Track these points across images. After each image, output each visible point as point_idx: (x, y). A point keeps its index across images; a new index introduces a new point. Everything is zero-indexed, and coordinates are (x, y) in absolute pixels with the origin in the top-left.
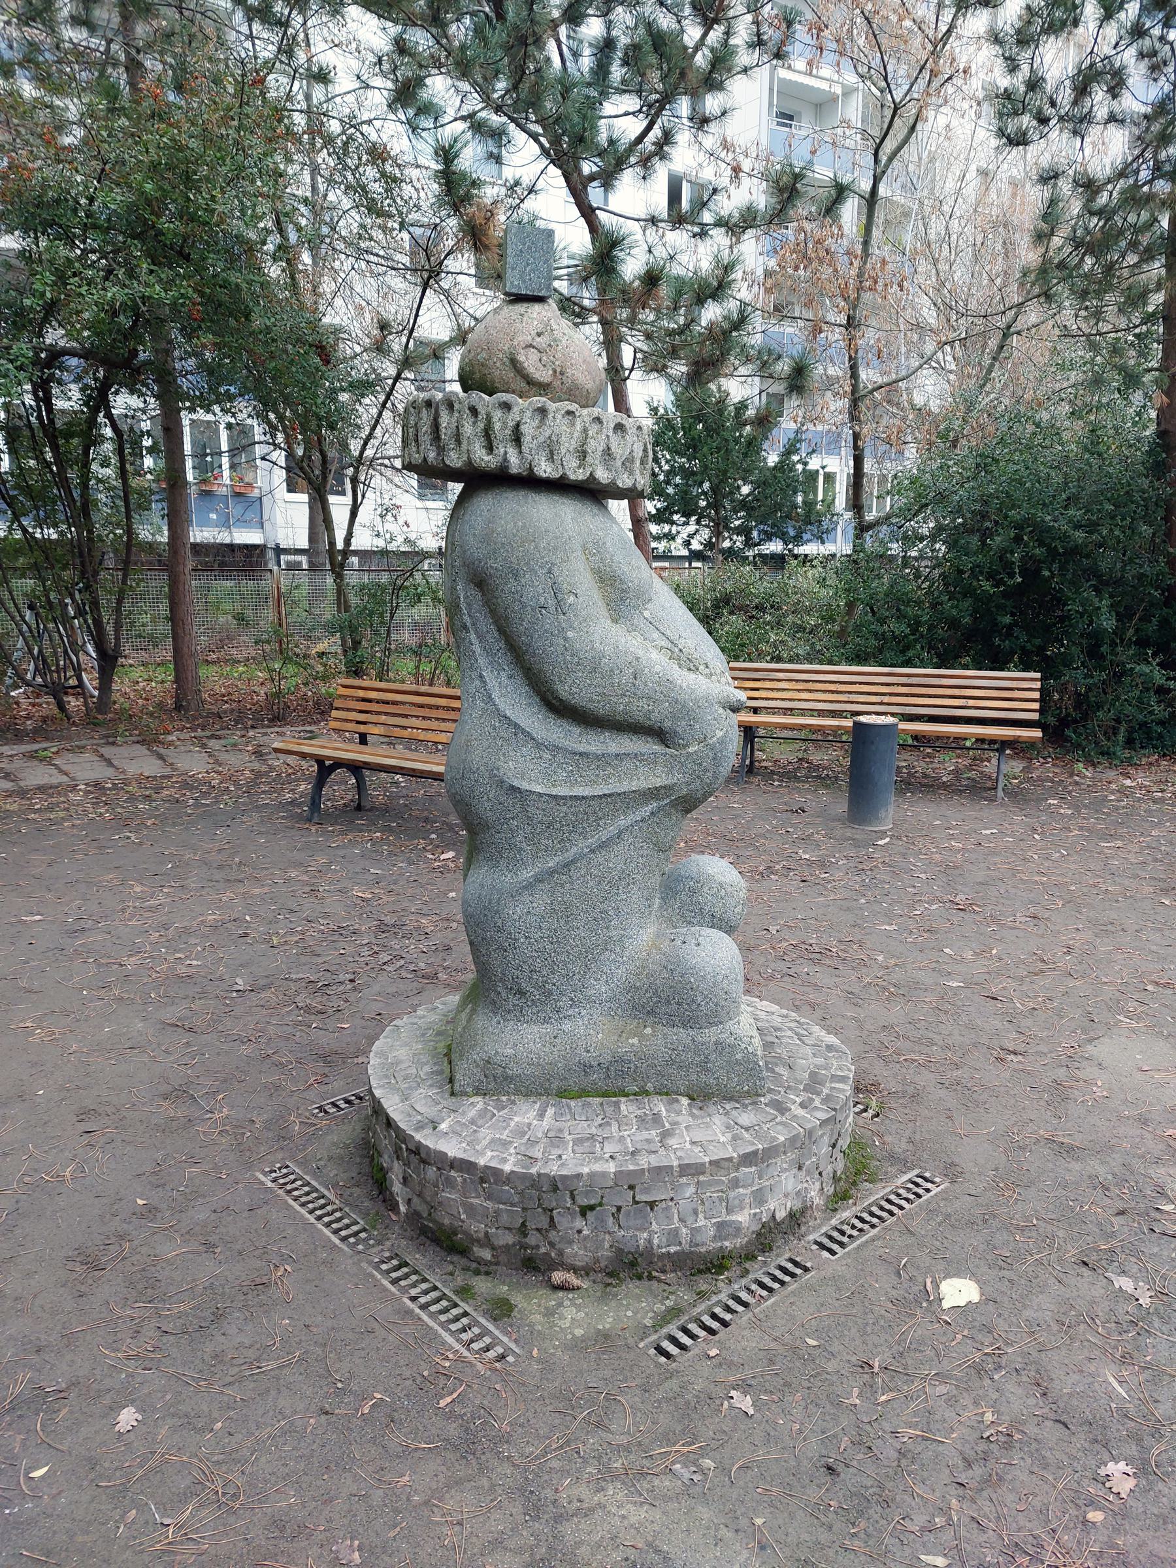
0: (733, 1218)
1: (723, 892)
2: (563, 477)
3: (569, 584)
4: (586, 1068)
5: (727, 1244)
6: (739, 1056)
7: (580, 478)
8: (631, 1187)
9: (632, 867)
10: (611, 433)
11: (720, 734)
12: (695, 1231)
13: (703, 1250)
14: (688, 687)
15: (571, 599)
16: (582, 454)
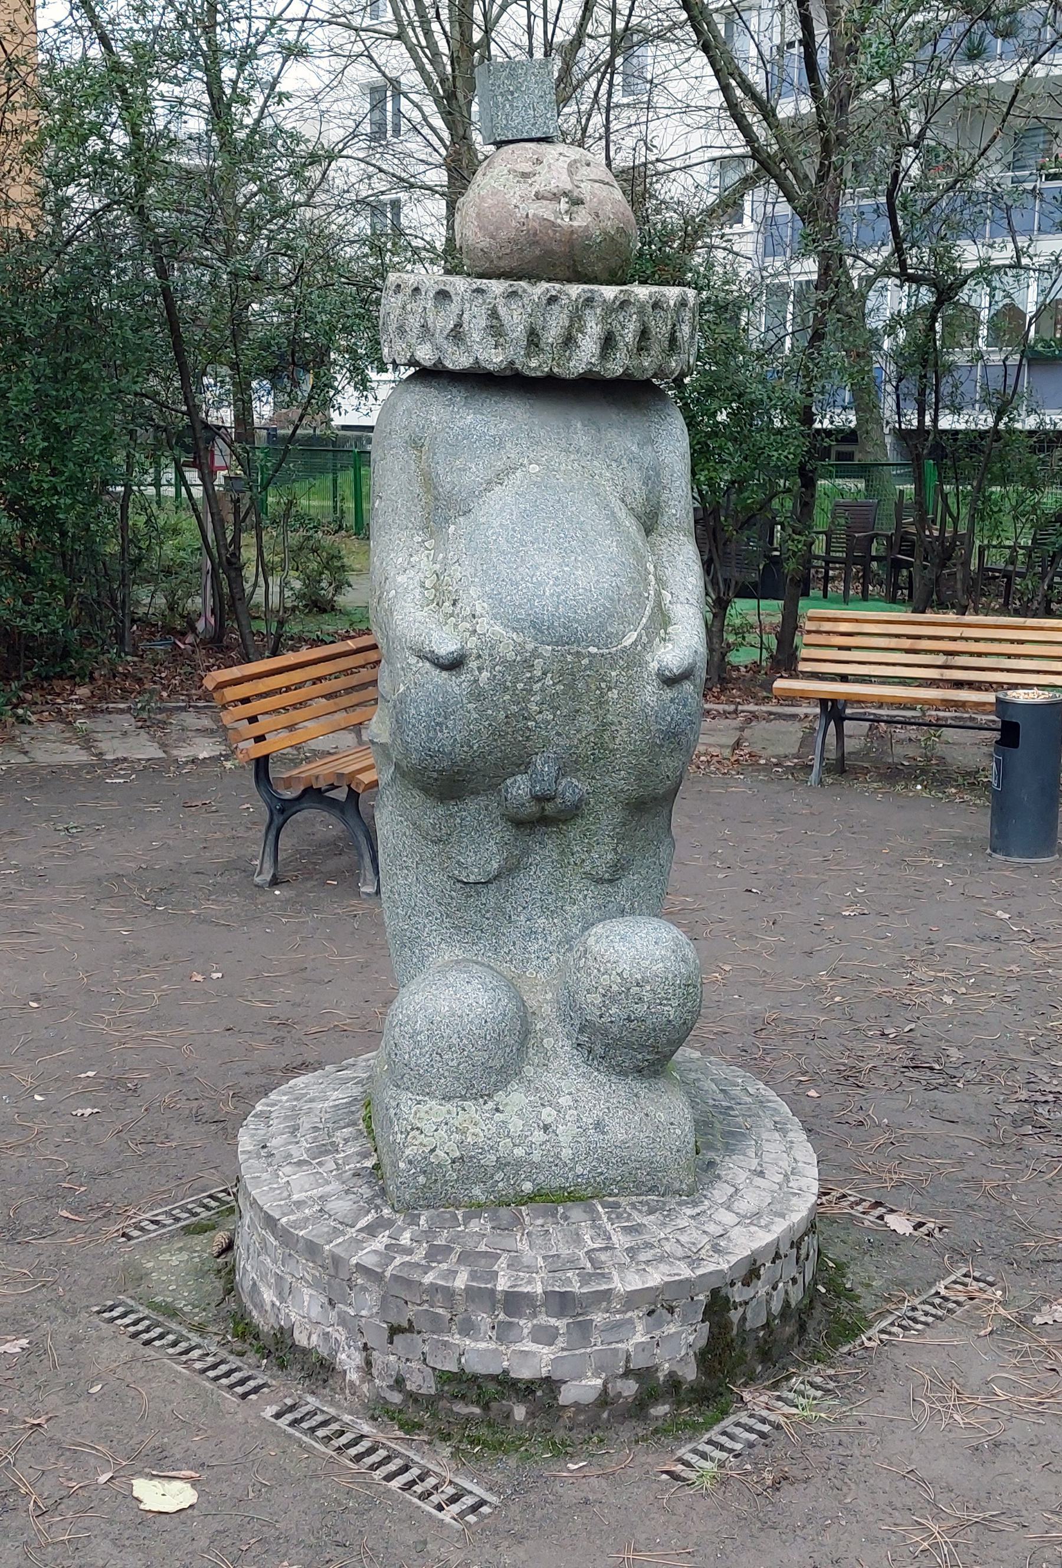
10: (430, 304)
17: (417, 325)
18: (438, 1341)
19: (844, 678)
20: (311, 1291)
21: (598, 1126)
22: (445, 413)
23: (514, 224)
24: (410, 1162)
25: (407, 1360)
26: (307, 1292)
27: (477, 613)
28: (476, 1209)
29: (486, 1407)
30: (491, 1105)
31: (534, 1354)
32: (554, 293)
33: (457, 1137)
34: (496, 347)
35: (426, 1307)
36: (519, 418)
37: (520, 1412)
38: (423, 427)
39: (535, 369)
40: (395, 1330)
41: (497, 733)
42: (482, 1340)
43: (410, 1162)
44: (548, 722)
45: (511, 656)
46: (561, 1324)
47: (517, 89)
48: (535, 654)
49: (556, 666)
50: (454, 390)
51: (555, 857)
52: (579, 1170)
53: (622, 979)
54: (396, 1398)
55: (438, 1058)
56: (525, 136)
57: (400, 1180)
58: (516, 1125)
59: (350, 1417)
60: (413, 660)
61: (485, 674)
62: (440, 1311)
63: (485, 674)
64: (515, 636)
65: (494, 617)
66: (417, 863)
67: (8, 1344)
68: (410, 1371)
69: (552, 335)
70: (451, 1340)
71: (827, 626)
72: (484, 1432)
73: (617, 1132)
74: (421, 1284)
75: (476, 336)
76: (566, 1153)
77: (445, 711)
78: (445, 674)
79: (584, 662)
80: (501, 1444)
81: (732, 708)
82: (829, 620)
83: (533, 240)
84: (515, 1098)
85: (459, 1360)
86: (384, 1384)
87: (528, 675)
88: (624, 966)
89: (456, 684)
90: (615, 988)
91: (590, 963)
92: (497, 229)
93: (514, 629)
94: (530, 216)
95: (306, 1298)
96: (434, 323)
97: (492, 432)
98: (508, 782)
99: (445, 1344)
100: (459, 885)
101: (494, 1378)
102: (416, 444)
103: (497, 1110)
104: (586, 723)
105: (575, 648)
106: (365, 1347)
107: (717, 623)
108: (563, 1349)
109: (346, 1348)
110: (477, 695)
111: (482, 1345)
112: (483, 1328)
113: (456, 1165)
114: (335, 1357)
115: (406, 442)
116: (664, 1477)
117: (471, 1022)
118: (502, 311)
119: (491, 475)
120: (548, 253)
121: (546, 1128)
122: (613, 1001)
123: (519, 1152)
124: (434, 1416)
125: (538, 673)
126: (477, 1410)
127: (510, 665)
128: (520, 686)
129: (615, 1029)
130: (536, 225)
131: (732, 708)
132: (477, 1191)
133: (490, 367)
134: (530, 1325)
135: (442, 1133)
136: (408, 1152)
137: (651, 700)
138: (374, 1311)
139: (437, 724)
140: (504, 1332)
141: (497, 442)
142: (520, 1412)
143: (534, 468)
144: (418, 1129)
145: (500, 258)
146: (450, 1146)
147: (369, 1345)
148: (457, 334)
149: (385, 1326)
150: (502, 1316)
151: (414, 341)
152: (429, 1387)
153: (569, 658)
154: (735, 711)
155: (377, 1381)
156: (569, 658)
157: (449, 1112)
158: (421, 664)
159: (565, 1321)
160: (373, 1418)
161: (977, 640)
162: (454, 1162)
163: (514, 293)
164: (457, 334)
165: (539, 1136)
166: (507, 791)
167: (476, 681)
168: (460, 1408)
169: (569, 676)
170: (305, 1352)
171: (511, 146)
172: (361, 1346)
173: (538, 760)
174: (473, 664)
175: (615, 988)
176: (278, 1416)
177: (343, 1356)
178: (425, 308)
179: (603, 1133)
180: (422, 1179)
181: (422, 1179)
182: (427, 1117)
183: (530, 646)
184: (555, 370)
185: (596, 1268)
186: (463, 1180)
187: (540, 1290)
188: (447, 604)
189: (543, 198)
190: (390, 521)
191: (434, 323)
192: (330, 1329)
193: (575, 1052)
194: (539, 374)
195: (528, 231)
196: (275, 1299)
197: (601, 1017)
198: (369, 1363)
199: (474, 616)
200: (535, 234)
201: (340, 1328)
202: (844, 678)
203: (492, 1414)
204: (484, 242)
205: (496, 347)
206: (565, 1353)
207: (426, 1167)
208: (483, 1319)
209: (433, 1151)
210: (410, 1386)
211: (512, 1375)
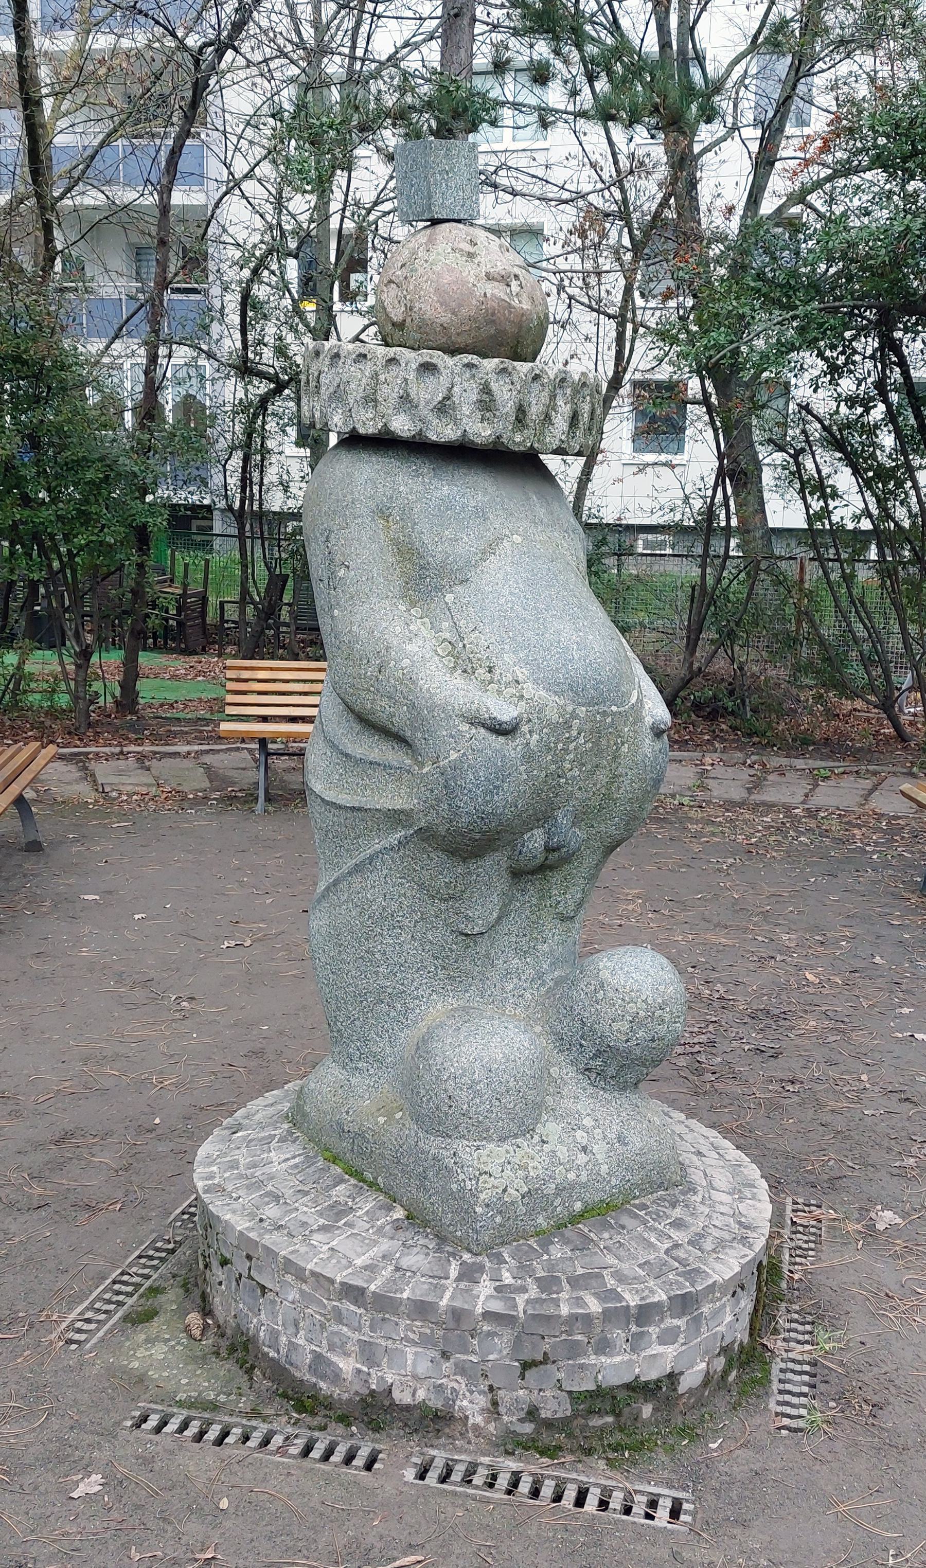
0: (334, 1359)
1: (600, 995)
2: (386, 430)
3: (343, 554)
4: (342, 1131)
5: (322, 1385)
6: (454, 1187)
7: (370, 431)
8: (249, 1257)
9: (394, 906)
10: (412, 376)
11: (454, 756)
12: (292, 1346)
13: (298, 1374)
14: (428, 690)
15: (342, 572)
16: (371, 400)
17: (395, 395)
18: (573, 1366)
19: (265, 719)
20: (414, 1349)
21: (621, 1139)
22: (417, 485)
23: (474, 302)
24: (487, 1206)
25: (540, 1390)
26: (410, 1351)
27: (520, 679)
28: (545, 1238)
29: (618, 1415)
30: (537, 1138)
31: (660, 1355)
32: (538, 372)
33: (521, 1173)
34: (482, 421)
35: (564, 1337)
36: (490, 491)
37: (647, 1411)
38: (392, 498)
39: (519, 444)
40: (526, 1366)
41: (537, 792)
42: (618, 1354)
43: (487, 1206)
44: (575, 778)
45: (555, 718)
46: (680, 1322)
47: (452, 169)
48: (574, 715)
49: (587, 727)
50: (419, 462)
51: (534, 901)
52: (614, 1181)
53: (648, 1004)
54: (528, 1428)
55: (498, 1103)
56: (456, 217)
57: (479, 1224)
58: (562, 1153)
59: (488, 1459)
60: (465, 727)
61: (535, 737)
62: (579, 1337)
63: (535, 737)
64: (557, 698)
65: (535, 682)
66: (416, 922)
67: (81, 1485)
68: (545, 1400)
69: (535, 411)
70: (587, 1362)
71: (246, 675)
72: (618, 1436)
73: (636, 1142)
74: (560, 1316)
75: (466, 410)
76: (604, 1168)
77: (502, 773)
78: (501, 739)
79: (609, 720)
80: (642, 1443)
81: (118, 750)
82: (246, 668)
83: (491, 318)
84: (551, 1128)
85: (596, 1377)
86: (514, 1419)
87: (567, 735)
88: (647, 993)
89: (511, 748)
90: (642, 1014)
91: (611, 994)
92: (460, 305)
93: (556, 693)
94: (488, 295)
95: (410, 1357)
96: (417, 394)
97: (473, 504)
98: (526, 837)
99: (582, 1367)
100: (460, 938)
101: (628, 1386)
102: (383, 513)
103: (543, 1142)
104: (602, 777)
105: (603, 708)
106: (491, 1388)
107: (81, 673)
108: (682, 1344)
109: (468, 1394)
110: (528, 757)
111: (617, 1359)
112: (618, 1343)
113: (526, 1200)
114: (452, 1406)
115: (373, 512)
116: (784, 1432)
117: (524, 1065)
118: (494, 386)
119: (483, 545)
120: (501, 332)
121: (584, 1149)
122: (641, 1025)
123: (571, 1176)
124: (570, 1436)
125: (574, 733)
126: (610, 1419)
127: (554, 727)
128: (560, 746)
129: (638, 1052)
130: (496, 305)
131: (118, 750)
132: (540, 1220)
133: (478, 440)
134: (657, 1330)
135: (508, 1172)
136: (482, 1196)
137: (648, 752)
138: (505, 1353)
139: (495, 787)
140: (636, 1343)
141: (481, 514)
142: (647, 1411)
143: (517, 539)
144: (486, 1173)
145: (458, 334)
146: (518, 1183)
147: (495, 1385)
148: (444, 408)
149: (516, 1364)
150: (634, 1328)
151: (390, 412)
152: (564, 1409)
153: (598, 717)
154: (122, 753)
155: (505, 1417)
156: (598, 717)
157: (507, 1152)
158: (474, 731)
159: (685, 1319)
160: (508, 1453)
161: (287, 681)
162: (523, 1197)
163: (504, 370)
164: (444, 408)
165: (582, 1158)
166: (523, 846)
167: (528, 744)
168: (596, 1422)
169: (596, 733)
170: (407, 1408)
171: (447, 224)
172: (486, 1389)
173: (559, 814)
174: (525, 728)
175: (642, 1014)
176: (422, 1476)
177: (465, 1403)
178: (406, 380)
179: (626, 1144)
180: (498, 1219)
181: (498, 1219)
182: (490, 1160)
183: (570, 709)
184: (536, 445)
185: (685, 1266)
186: (531, 1212)
187: (665, 1297)
188: (481, 671)
189: (493, 279)
190: (367, 590)
191: (417, 394)
192: (444, 1381)
193: (581, 1077)
194: (522, 448)
195: (487, 310)
196: (359, 1366)
197: (627, 1041)
198: (495, 1404)
199: (517, 682)
200: (493, 314)
201: (459, 1378)
202: (265, 719)
203: (623, 1420)
204: (445, 318)
205: (482, 421)
206: (684, 1348)
207: (501, 1207)
208: (618, 1335)
209: (505, 1191)
210: (544, 1414)
211: (643, 1379)
